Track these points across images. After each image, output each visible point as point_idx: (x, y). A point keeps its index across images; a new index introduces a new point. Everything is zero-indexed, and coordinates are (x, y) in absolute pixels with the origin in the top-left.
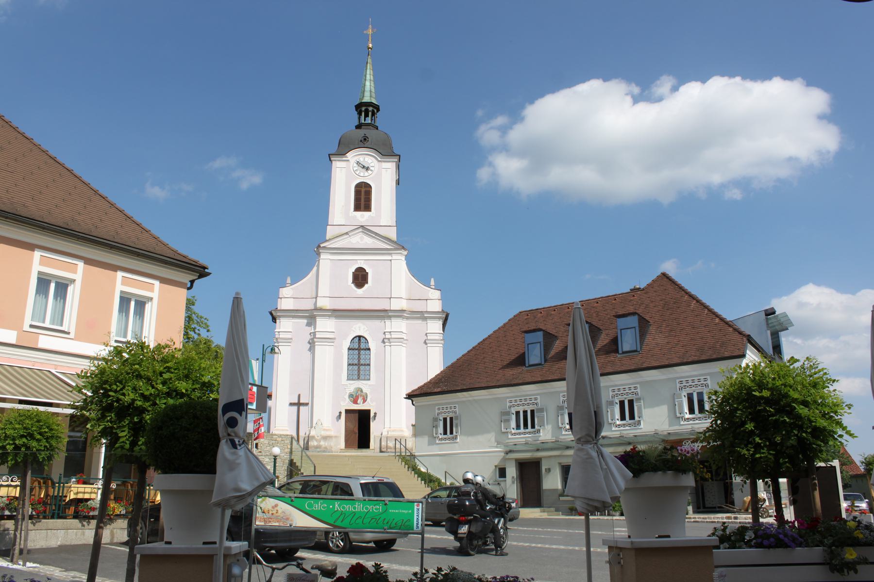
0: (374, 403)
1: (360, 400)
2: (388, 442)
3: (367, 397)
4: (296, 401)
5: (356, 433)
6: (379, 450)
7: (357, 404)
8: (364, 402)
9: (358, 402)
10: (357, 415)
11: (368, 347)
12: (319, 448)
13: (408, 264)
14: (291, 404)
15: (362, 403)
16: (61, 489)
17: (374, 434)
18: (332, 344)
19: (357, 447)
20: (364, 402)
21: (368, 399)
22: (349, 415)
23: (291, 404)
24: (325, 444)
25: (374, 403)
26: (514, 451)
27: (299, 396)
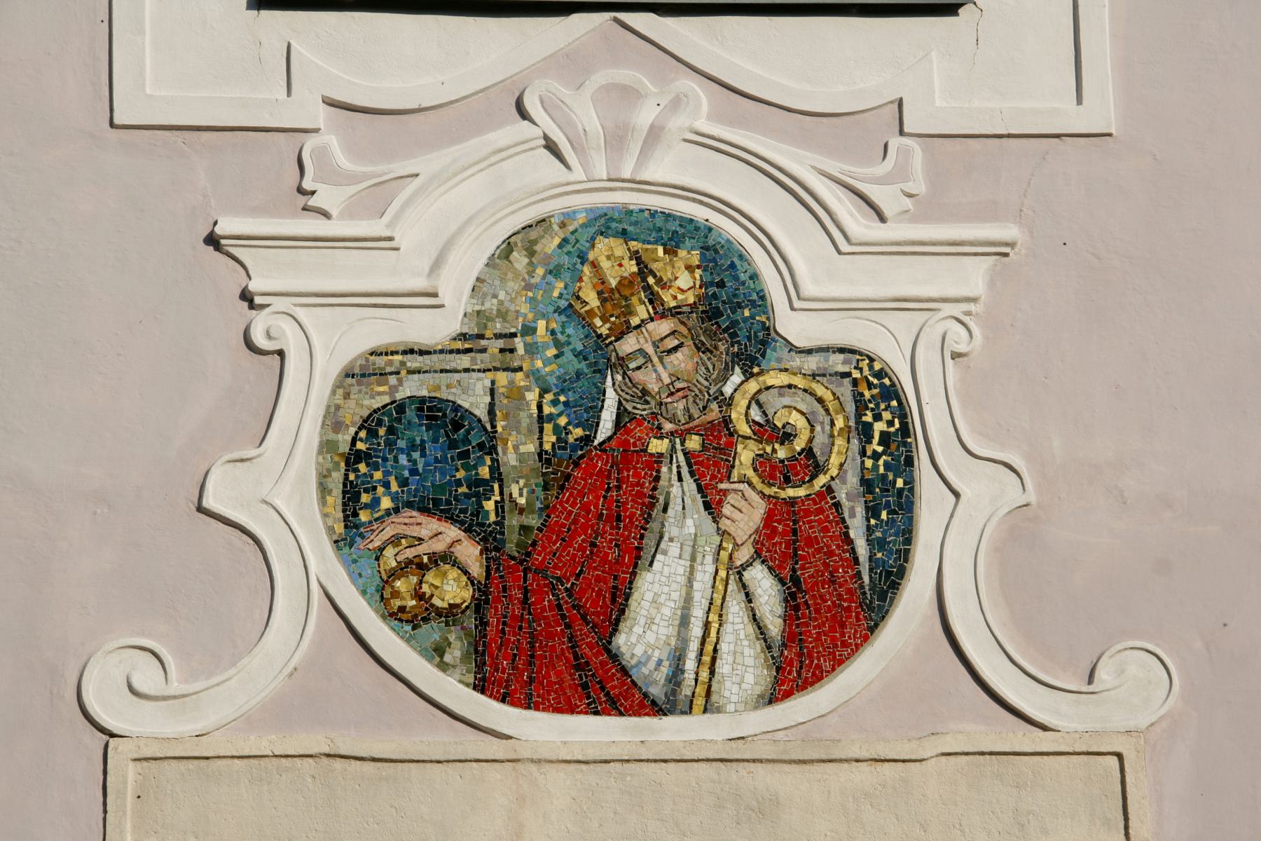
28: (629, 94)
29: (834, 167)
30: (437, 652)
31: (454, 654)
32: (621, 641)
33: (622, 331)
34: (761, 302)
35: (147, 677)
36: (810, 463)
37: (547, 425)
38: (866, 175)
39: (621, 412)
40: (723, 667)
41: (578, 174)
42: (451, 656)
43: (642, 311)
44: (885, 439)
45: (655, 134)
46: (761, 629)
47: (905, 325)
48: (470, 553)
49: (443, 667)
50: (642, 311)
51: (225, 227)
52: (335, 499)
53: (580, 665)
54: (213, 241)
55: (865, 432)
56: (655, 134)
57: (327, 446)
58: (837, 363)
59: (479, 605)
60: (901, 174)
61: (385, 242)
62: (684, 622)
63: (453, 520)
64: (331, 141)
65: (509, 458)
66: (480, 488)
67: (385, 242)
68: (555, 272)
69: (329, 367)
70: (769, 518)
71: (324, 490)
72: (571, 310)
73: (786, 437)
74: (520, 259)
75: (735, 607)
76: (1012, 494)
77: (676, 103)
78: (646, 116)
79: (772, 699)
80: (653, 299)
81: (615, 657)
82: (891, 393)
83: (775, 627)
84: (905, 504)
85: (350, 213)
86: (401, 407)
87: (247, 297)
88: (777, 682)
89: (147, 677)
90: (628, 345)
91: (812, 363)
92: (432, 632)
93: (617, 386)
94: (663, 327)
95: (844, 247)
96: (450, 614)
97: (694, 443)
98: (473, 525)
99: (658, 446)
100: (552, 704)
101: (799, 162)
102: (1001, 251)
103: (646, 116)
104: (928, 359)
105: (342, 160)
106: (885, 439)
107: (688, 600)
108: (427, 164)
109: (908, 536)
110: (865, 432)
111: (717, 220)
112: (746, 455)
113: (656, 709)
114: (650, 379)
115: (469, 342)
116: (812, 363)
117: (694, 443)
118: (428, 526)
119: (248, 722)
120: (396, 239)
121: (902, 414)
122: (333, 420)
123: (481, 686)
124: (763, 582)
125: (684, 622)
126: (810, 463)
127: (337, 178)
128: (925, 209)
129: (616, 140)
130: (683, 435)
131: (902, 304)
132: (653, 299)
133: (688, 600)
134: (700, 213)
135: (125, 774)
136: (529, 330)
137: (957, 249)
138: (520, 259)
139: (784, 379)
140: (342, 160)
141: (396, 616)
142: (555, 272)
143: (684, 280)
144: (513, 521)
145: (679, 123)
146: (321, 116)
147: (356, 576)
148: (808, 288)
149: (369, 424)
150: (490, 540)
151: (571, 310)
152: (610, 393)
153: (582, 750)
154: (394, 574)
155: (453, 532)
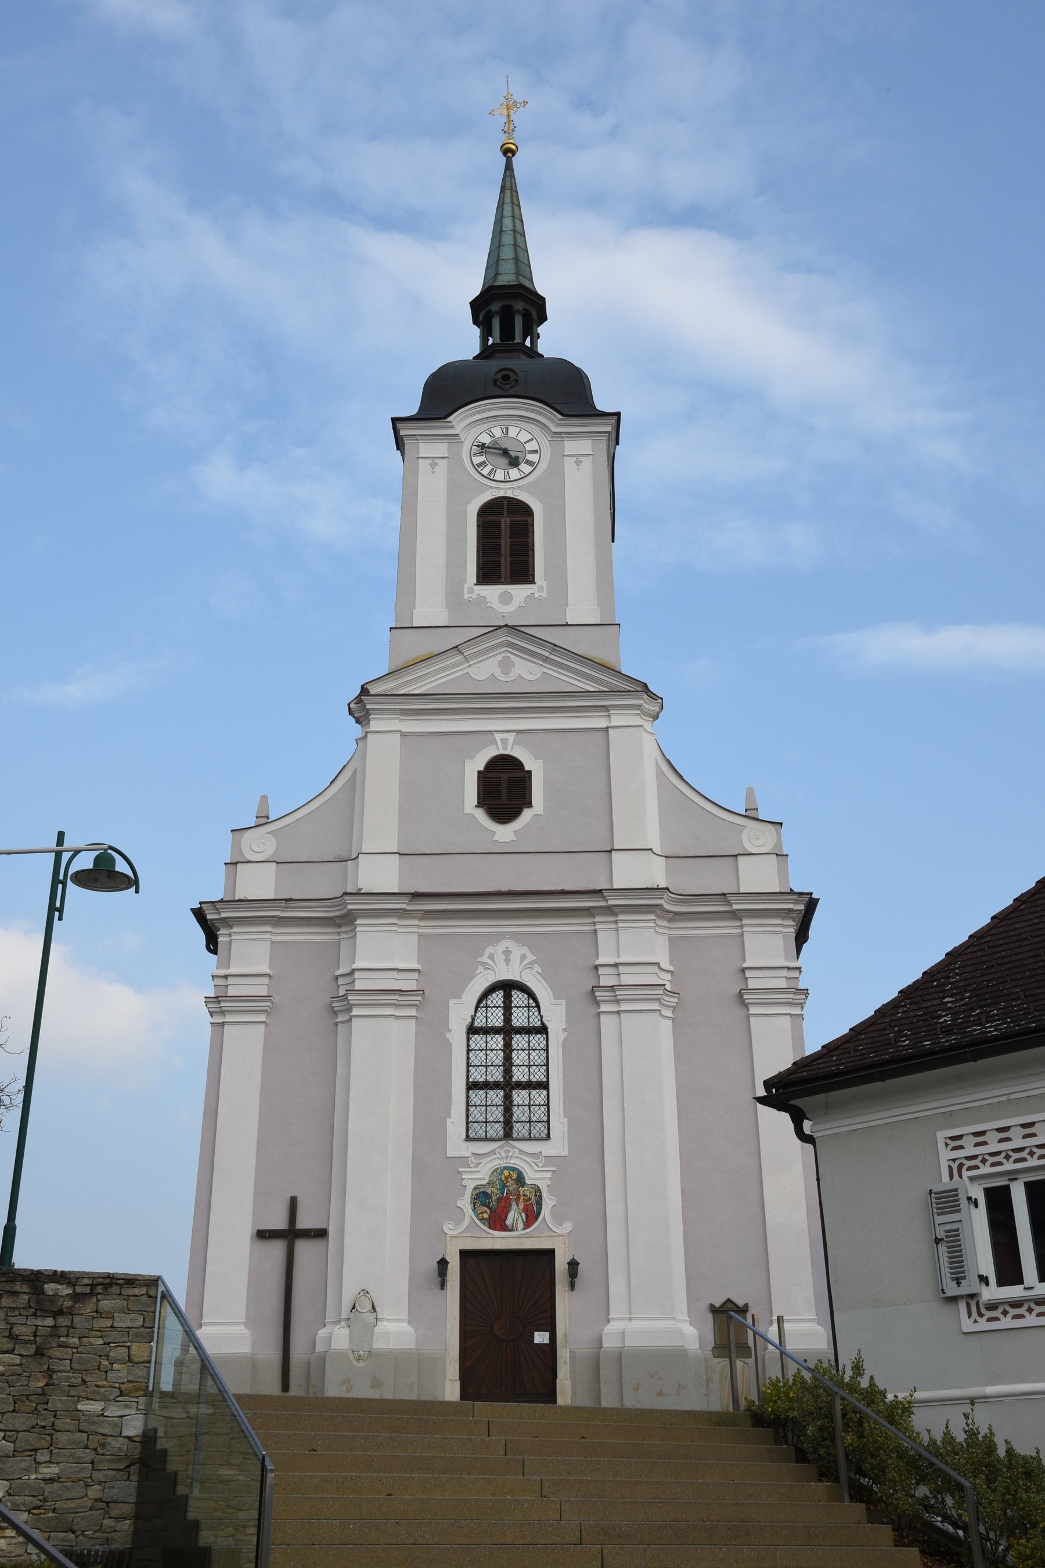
29: (534, 1160)
30: (484, 1224)
31: (486, 1224)
32: (506, 1222)
33: (507, 1182)
34: (524, 1178)
39: (507, 1193)
40: (518, 1225)
41: (502, 1162)
42: (486, 1224)
43: (510, 1180)
44: (539, 1196)
46: (523, 1220)
48: (488, 1211)
49: (485, 1226)
50: (510, 1180)
52: (472, 1205)
53: (501, 1225)
55: (536, 1195)
56: (511, 1157)
57: (471, 1198)
58: (533, 1186)
59: (489, 1218)
60: (541, 1162)
62: (514, 1220)
63: (486, 1207)
65: (493, 1199)
66: (490, 1203)
67: (478, 1171)
68: (499, 1175)
70: (524, 1207)
71: (471, 1203)
72: (501, 1180)
73: (527, 1196)
74: (495, 1173)
75: (520, 1218)
78: (510, 1154)
80: (511, 1178)
81: (505, 1224)
82: (540, 1190)
83: (525, 1220)
84: (541, 1204)
86: (480, 1192)
88: (525, 1225)
90: (508, 1184)
91: (530, 1186)
92: (484, 1221)
94: (512, 1182)
96: (486, 1219)
97: (515, 1197)
98: (489, 1207)
99: (511, 1197)
100: (816, 1529)
103: (510, 1154)
106: (539, 1196)
107: (514, 1217)
109: (541, 1211)
110: (536, 1195)
111: (519, 1168)
112: (522, 1198)
113: (511, 1231)
114: (510, 1189)
115: (488, 1184)
116: (530, 1186)
117: (515, 1197)
118: (484, 1208)
121: (541, 1193)
122: (472, 1194)
123: (489, 1228)
124: (523, 1215)
125: (514, 1220)
126: (530, 1199)
127: (472, 1163)
130: (514, 1196)
132: (511, 1178)
133: (514, 1217)
134: (517, 1167)
136: (496, 1182)
138: (495, 1173)
139: (526, 1188)
142: (499, 1175)
143: (515, 1176)
144: (494, 1207)
145: (514, 1155)
147: (475, 1214)
149: (476, 1195)
150: (491, 1209)
151: (501, 1180)
152: (506, 1191)
153: (661, 1379)
154: (480, 1214)
155: (486, 1208)
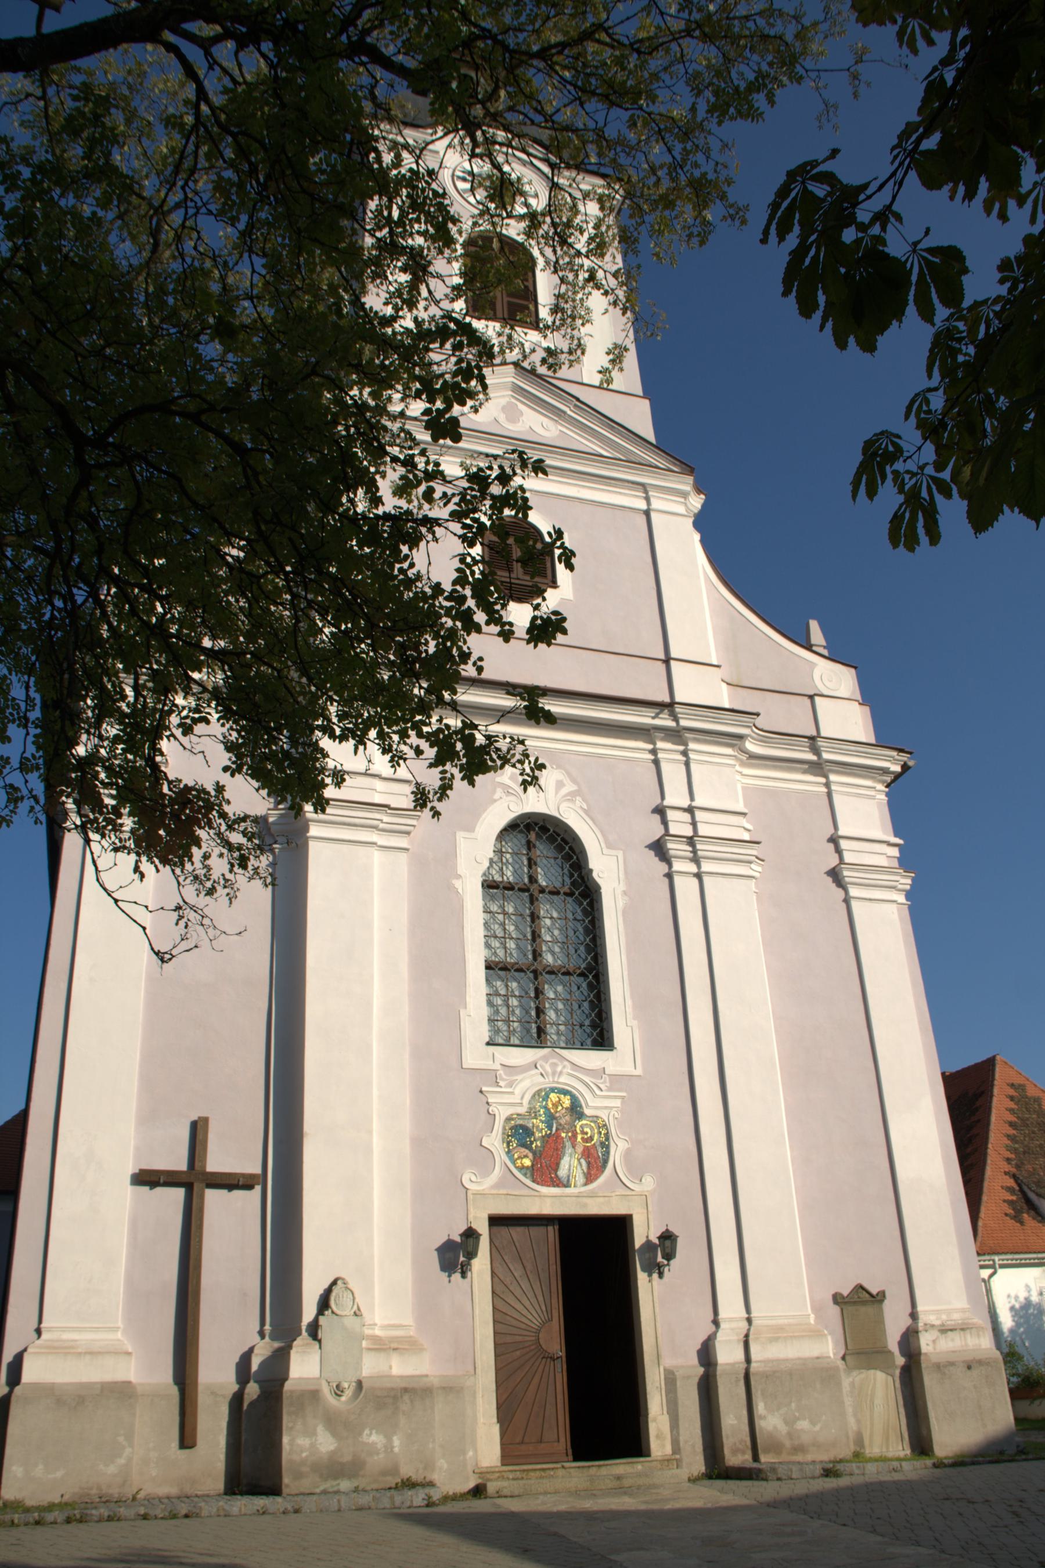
0: (648, 1183)
1: (571, 1164)
2: (760, 1408)
3: (605, 1146)
4: (179, 1162)
5: (658, 1437)
6: (697, 1464)
7: (557, 1182)
8: (590, 1177)
9: (562, 1172)
10: (552, 1233)
11: (493, 898)
12: (351, 1476)
13: (706, 544)
14: (146, 1179)
15: (580, 1179)
16: (643, 718)
17: (668, 1362)
18: (402, 842)
19: (564, 1443)
20: (590, 1177)
21: (616, 1155)
22: (504, 1231)
23: (146, 1179)
24: (388, 1448)
25: (648, 1183)
26: (989, 1307)
27: (198, 1131)
28: (555, 1065)
30: (525, 1175)
34: (581, 1107)
35: (474, 1178)
36: (591, 1138)
37: (364, 1368)
38: (598, 1082)
45: (561, 1073)
47: (606, 1112)
51: (484, 1089)
54: (481, 1092)
56: (561, 1073)
60: (605, 1082)
61: (512, 1093)
64: (501, 1072)
69: (503, 1118)
76: (627, 1146)
77: (564, 1067)
78: (559, 1069)
79: (586, 1184)
82: (605, 1125)
84: (608, 1147)
85: (506, 1087)
87: (488, 1103)
89: (474, 1178)
92: (524, 1171)
93: (753, 858)
95: (598, 1092)
96: (527, 1168)
101: (587, 1079)
102: (623, 1098)
103: (559, 1069)
104: (611, 1118)
105: (504, 1077)
108: (519, 1077)
112: (579, 1137)
119: (493, 1187)
120: (933, 547)
122: (504, 1128)
123: (534, 1181)
124: (583, 1161)
128: (610, 1089)
129: (554, 1073)
131: (606, 1108)
135: (470, 1197)
137: (616, 1097)
140: (504, 1077)
141: (517, 1168)
146: (499, 1067)
148: (590, 1104)
